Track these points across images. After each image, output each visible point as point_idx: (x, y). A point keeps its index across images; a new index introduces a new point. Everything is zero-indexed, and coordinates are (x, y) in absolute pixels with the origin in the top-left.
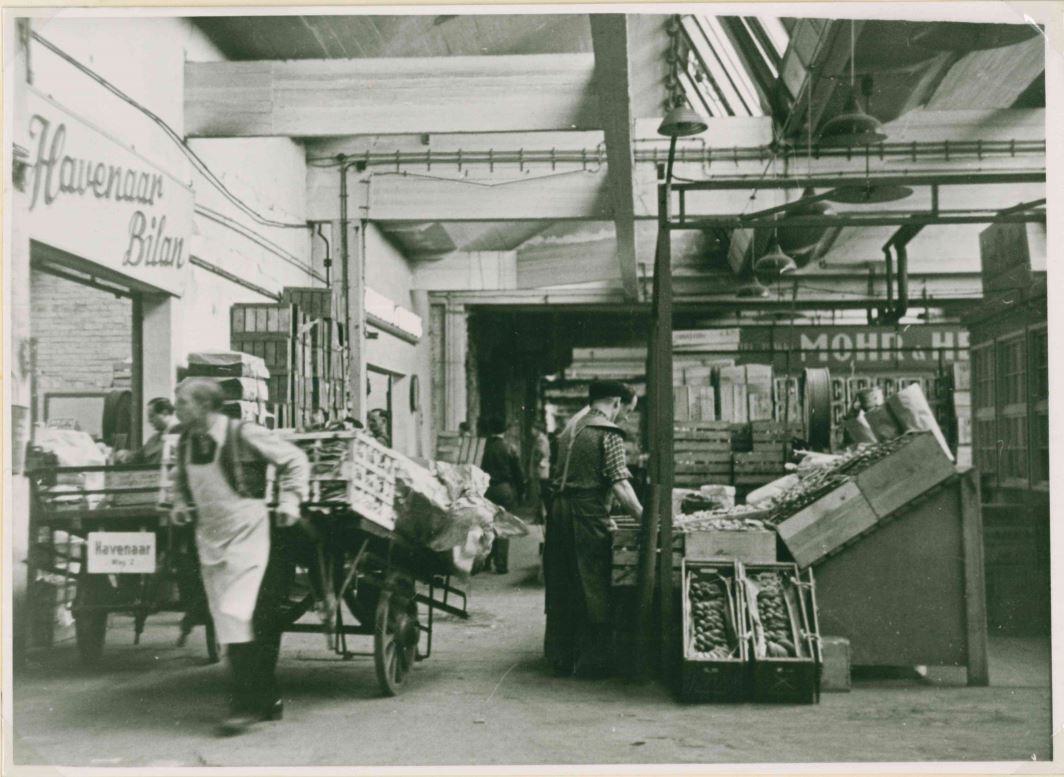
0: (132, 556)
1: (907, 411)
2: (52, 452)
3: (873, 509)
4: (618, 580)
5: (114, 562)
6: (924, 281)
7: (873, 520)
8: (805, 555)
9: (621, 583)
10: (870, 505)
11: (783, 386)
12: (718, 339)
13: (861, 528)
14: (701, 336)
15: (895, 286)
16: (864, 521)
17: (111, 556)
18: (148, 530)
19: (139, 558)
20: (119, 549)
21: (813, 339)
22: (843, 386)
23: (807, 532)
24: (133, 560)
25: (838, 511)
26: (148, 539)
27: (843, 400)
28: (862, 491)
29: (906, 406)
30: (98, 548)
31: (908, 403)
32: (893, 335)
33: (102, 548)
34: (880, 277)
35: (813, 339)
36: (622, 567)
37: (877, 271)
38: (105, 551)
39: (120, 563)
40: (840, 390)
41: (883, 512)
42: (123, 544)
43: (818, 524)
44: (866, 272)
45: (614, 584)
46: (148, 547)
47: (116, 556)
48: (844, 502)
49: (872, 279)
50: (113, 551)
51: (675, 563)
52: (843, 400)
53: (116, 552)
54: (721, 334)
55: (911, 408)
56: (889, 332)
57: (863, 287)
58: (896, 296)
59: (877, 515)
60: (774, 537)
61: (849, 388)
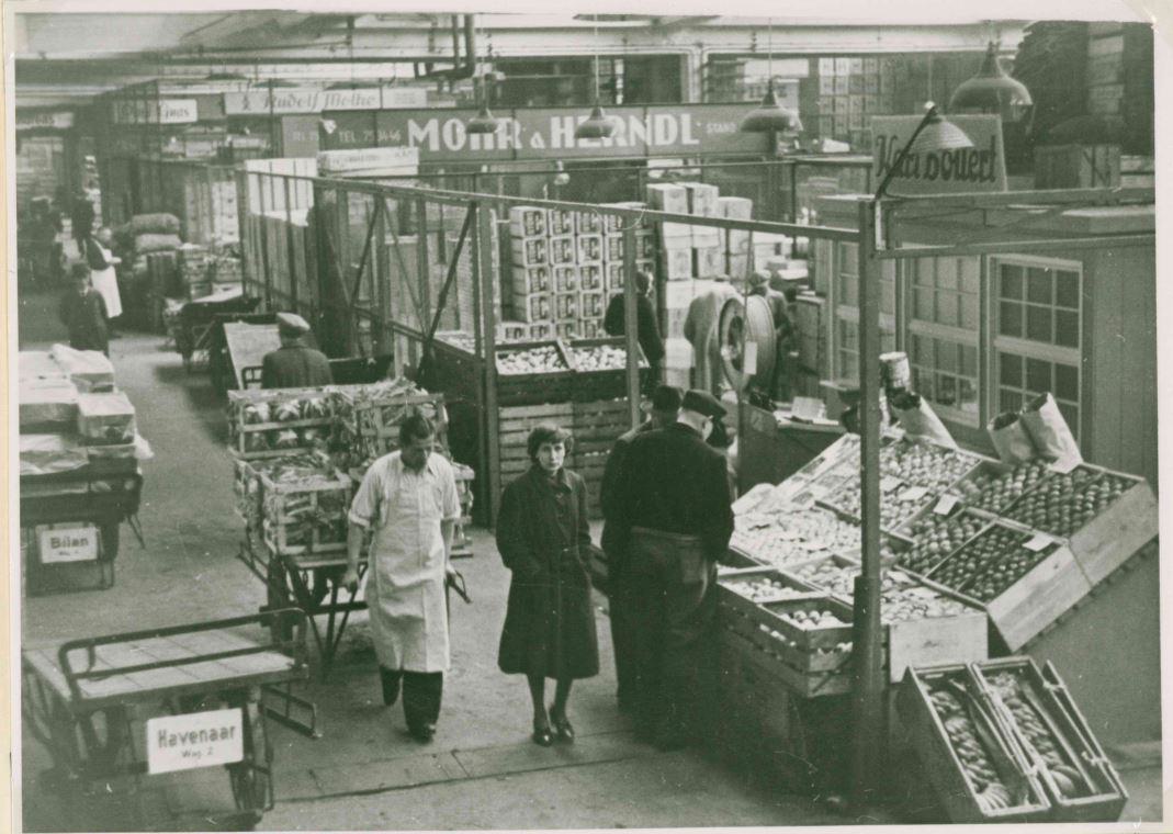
0: (210, 743)
1: (1049, 429)
2: (432, 740)
3: (1087, 577)
4: (815, 690)
5: (186, 754)
6: (489, 36)
7: (1086, 590)
8: (1014, 637)
9: (817, 694)
10: (1083, 573)
11: (532, 247)
12: (396, 162)
13: (1075, 599)
14: (373, 158)
15: (462, 40)
16: (1077, 591)
17: (180, 748)
18: (231, 706)
19: (219, 744)
20: (192, 737)
21: (422, 125)
22: (545, 217)
23: (1019, 610)
24: (211, 748)
25: (1052, 581)
26: (231, 718)
27: (544, 233)
28: (1075, 556)
29: (1047, 424)
30: (162, 738)
31: (1049, 421)
32: (509, 120)
33: (168, 738)
34: (444, 31)
35: (422, 125)
36: (818, 674)
37: (440, 25)
38: (173, 742)
39: (195, 754)
40: (542, 222)
41: (1096, 579)
42: (197, 729)
43: (1030, 600)
44: (428, 25)
45: (811, 695)
46: (232, 729)
47: (188, 746)
48: (1058, 570)
49: (433, 32)
50: (183, 740)
51: (689, 577)
52: (544, 233)
53: (188, 740)
54: (397, 155)
55: (1053, 427)
56: (504, 116)
57: (424, 41)
58: (463, 53)
59: (1090, 583)
60: (985, 619)
61: (550, 219)
